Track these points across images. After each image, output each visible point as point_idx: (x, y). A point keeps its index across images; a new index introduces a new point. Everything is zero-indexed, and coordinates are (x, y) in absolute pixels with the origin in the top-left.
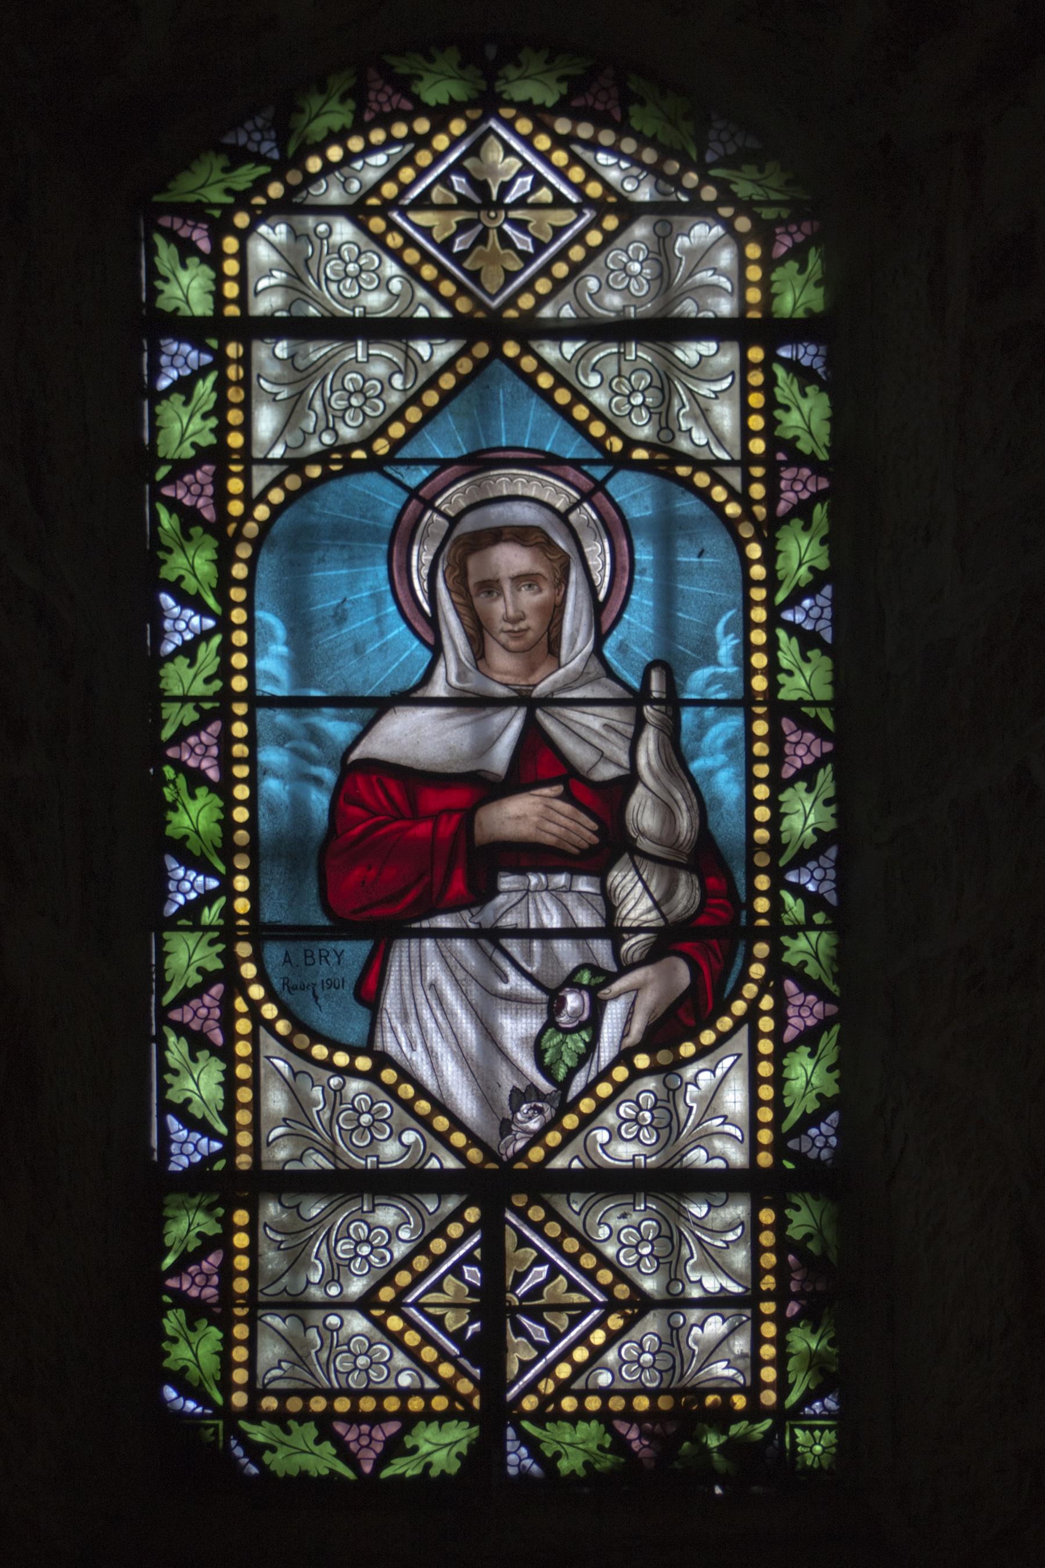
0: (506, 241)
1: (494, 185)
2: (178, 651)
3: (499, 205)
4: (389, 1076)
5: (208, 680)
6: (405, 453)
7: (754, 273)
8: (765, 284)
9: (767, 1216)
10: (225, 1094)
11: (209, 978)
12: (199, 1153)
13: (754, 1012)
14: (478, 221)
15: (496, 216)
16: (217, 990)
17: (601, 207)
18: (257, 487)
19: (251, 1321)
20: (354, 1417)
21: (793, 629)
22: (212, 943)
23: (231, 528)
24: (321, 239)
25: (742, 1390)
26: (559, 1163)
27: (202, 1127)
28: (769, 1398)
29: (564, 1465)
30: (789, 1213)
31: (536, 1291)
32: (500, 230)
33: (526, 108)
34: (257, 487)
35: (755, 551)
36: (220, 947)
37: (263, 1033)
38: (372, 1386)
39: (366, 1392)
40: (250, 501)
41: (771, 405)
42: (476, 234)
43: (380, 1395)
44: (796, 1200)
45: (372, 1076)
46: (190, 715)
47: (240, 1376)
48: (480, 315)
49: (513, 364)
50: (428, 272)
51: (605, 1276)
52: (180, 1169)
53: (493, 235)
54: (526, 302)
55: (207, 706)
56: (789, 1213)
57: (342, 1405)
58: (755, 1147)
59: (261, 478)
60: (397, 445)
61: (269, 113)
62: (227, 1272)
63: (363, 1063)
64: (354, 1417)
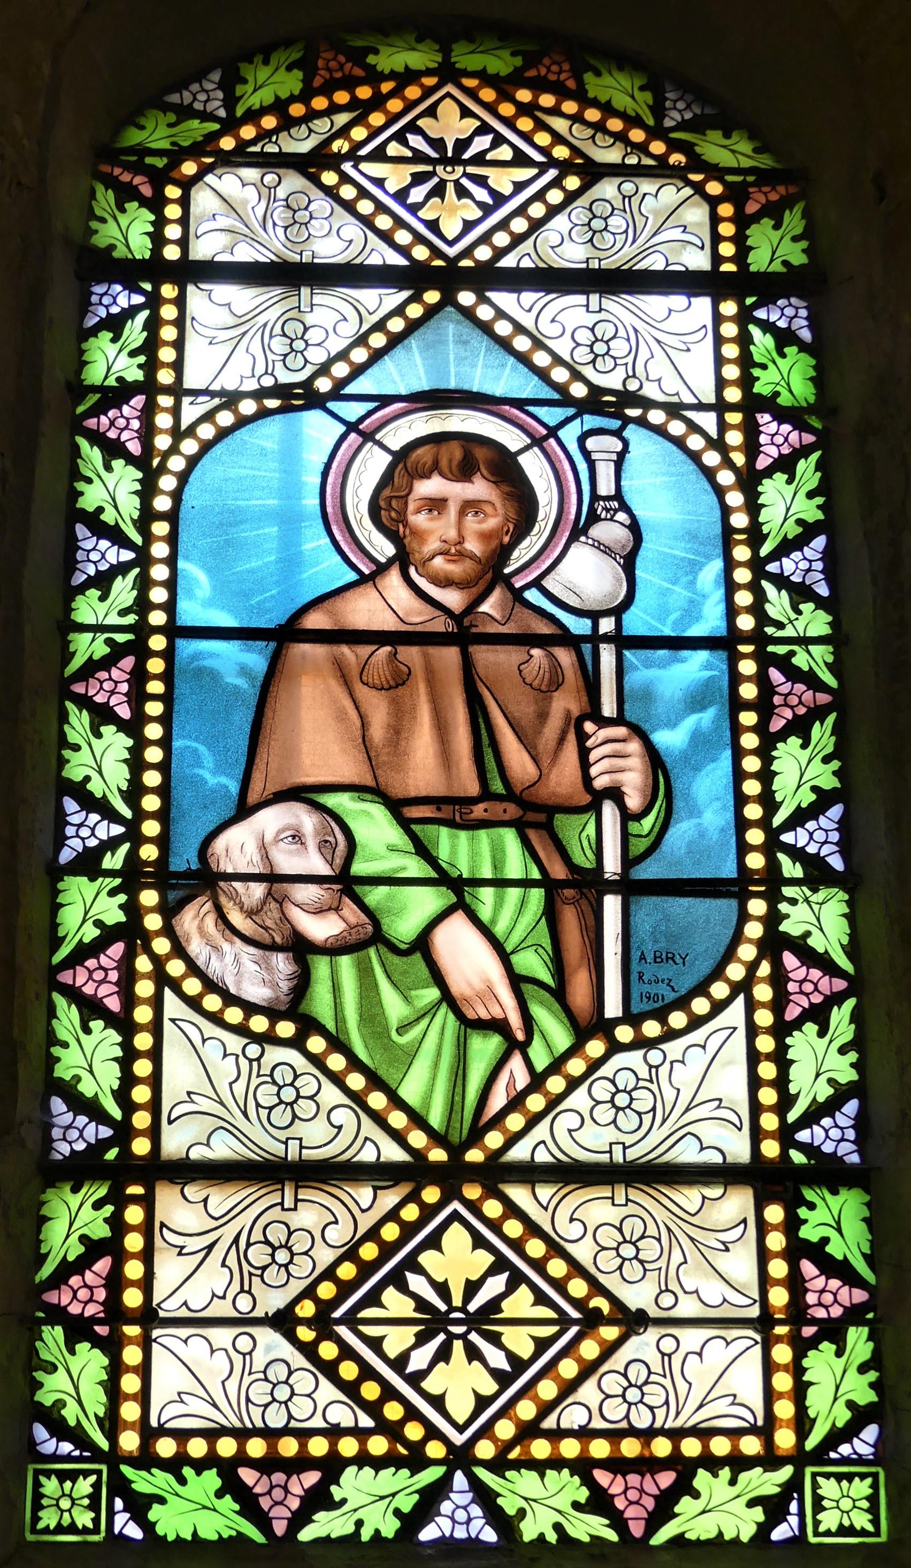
0: (462, 192)
1: (450, 142)
2: (91, 582)
3: (456, 160)
4: (316, 1044)
5: (123, 613)
6: (349, 390)
7: (727, 229)
8: (739, 240)
9: (774, 1213)
10: (122, 1071)
11: (109, 935)
12: (85, 1141)
13: (744, 987)
14: (434, 173)
15: (454, 170)
16: (117, 950)
17: (565, 168)
18: (187, 418)
19: (146, 1343)
20: (267, 1465)
21: (781, 581)
22: (112, 893)
23: (156, 462)
24: (270, 188)
25: (752, 1430)
26: (508, 262)
27: (93, 1110)
28: (785, 1439)
29: (529, 1531)
30: (803, 1212)
31: (494, 1305)
32: (457, 183)
33: (486, 78)
34: (187, 418)
35: (735, 499)
36: (122, 898)
37: (169, 995)
38: (293, 1424)
39: (286, 1431)
40: (178, 434)
41: (746, 361)
42: (427, 152)
43: (303, 1435)
44: (809, 1194)
45: (297, 1043)
46: (100, 650)
47: (130, 1411)
48: (438, 263)
49: (468, 314)
50: (384, 222)
51: (578, 1288)
52: (61, 1157)
53: (450, 188)
54: (483, 253)
55: (121, 638)
56: (803, 1212)
57: (256, 1448)
58: (757, 1135)
59: (190, 412)
60: (341, 383)
61: (216, 76)
62: (115, 1282)
63: (286, 1029)
64: (267, 1465)
